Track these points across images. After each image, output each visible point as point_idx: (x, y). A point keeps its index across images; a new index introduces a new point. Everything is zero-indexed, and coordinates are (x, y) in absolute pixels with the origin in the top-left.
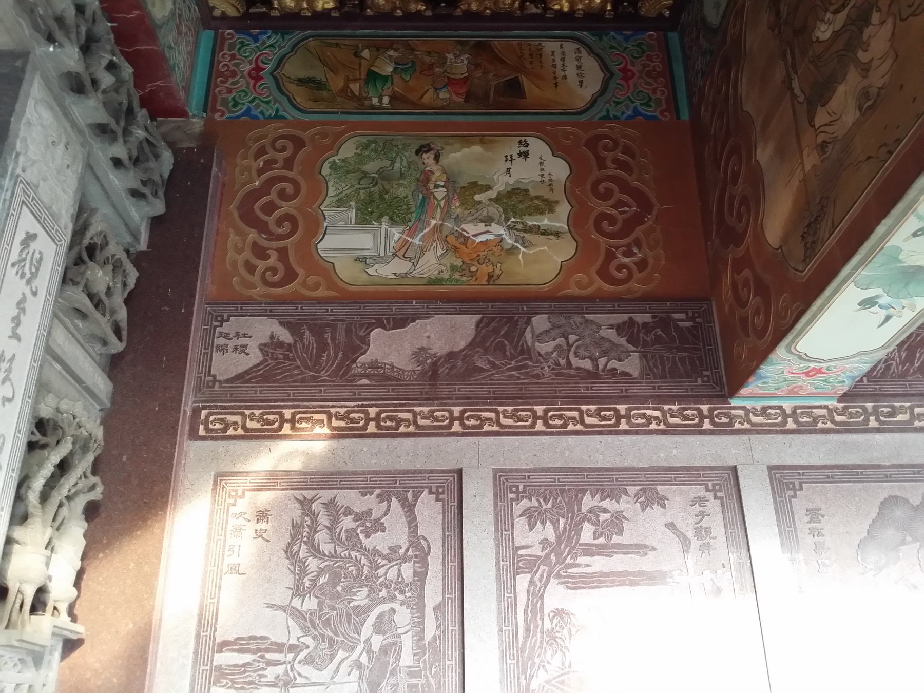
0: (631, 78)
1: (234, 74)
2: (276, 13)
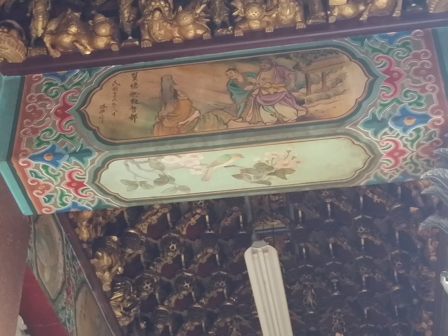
1: (417, 72)
2: (147, 44)
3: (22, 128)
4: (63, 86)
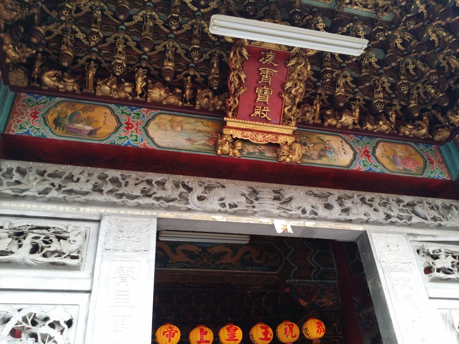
0: (131, 128)
3: (13, 118)
4: (37, 102)
